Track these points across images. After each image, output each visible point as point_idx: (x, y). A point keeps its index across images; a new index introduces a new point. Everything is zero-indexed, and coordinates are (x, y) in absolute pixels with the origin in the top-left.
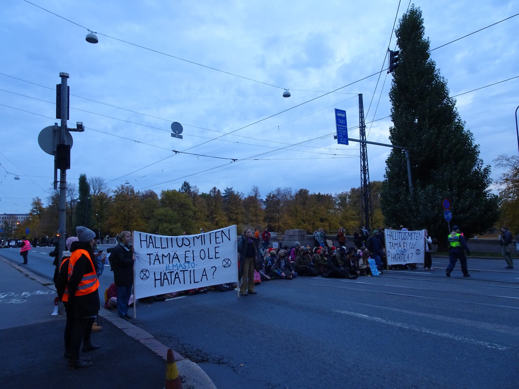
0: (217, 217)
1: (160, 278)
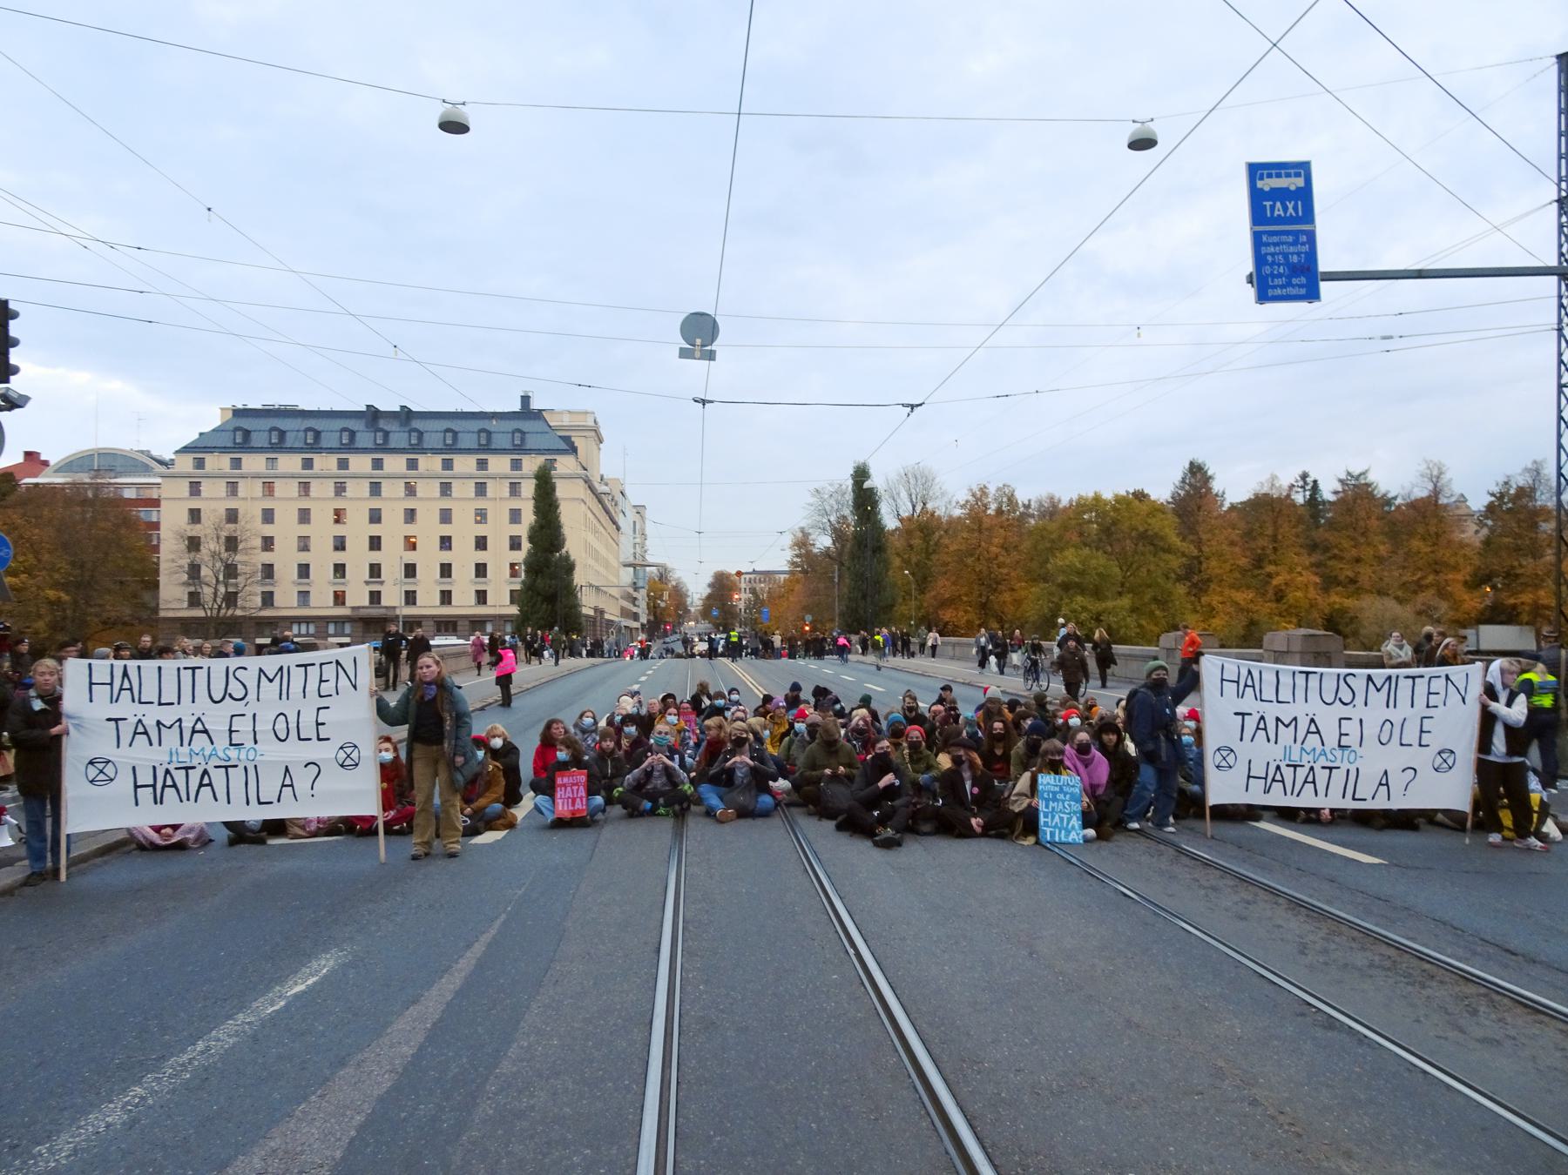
0: (1278, 574)
1: (151, 782)
